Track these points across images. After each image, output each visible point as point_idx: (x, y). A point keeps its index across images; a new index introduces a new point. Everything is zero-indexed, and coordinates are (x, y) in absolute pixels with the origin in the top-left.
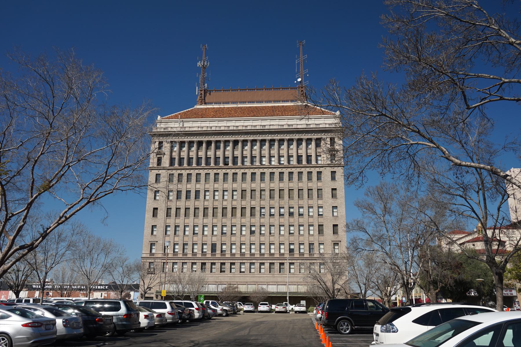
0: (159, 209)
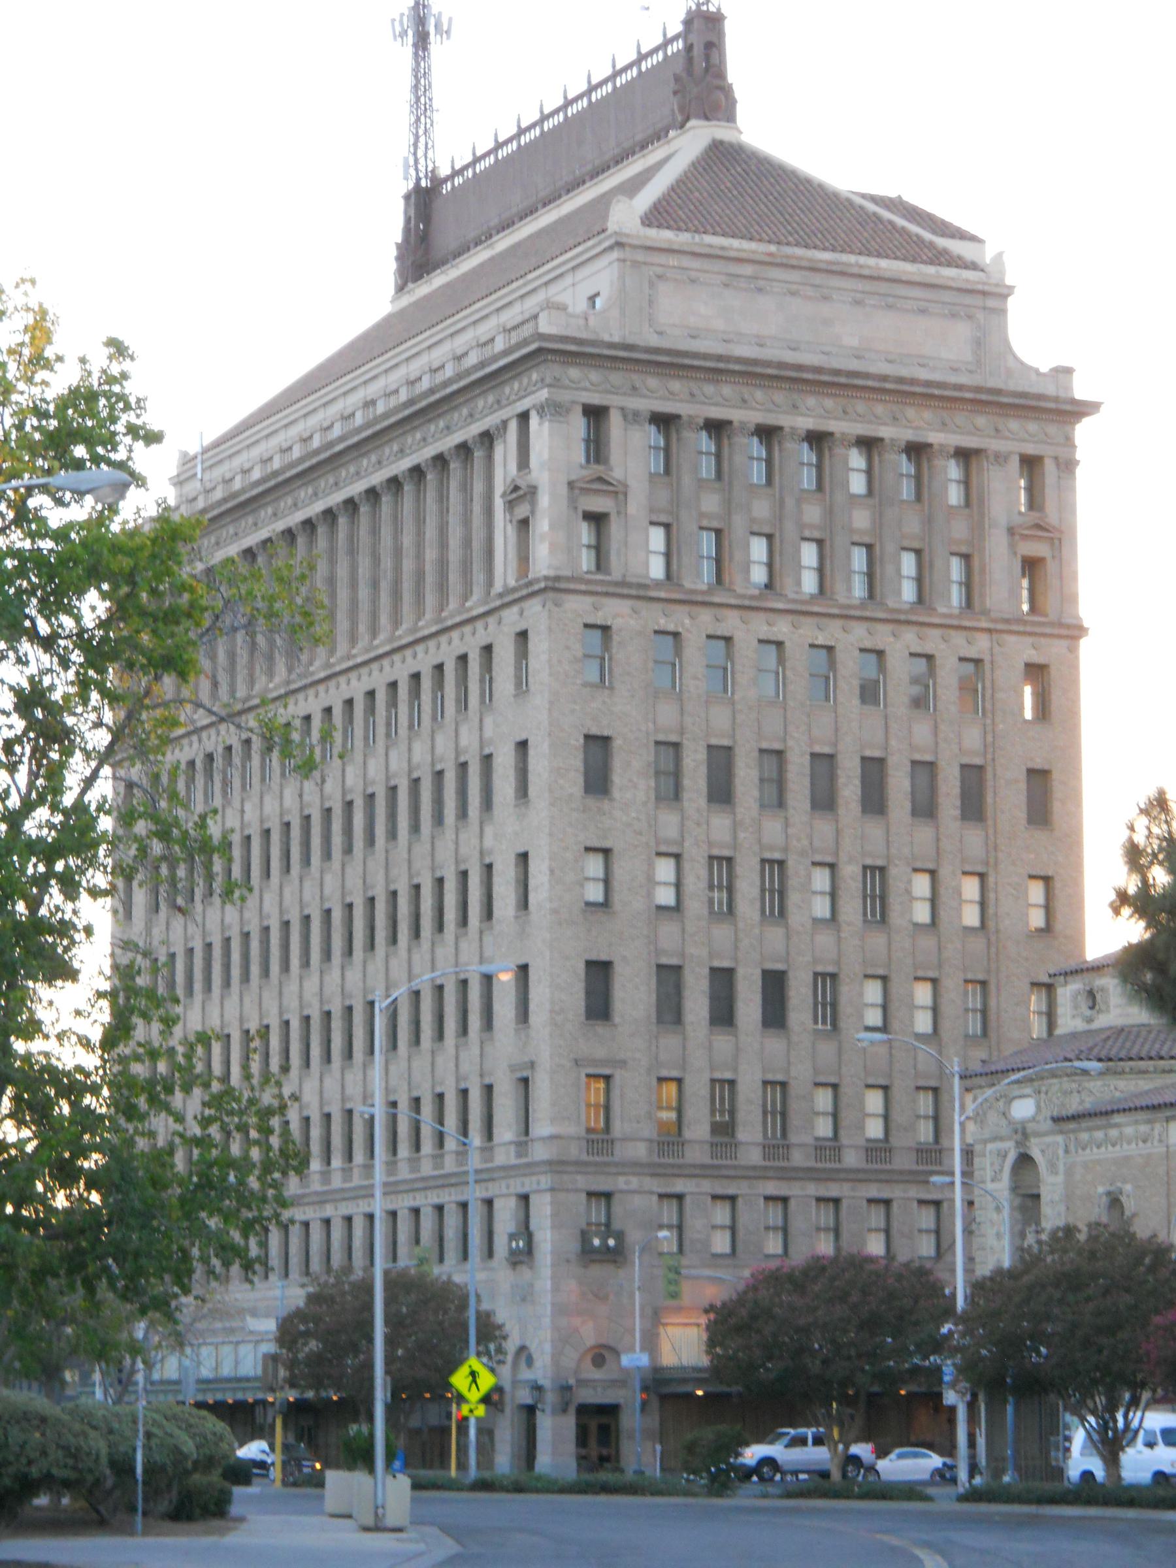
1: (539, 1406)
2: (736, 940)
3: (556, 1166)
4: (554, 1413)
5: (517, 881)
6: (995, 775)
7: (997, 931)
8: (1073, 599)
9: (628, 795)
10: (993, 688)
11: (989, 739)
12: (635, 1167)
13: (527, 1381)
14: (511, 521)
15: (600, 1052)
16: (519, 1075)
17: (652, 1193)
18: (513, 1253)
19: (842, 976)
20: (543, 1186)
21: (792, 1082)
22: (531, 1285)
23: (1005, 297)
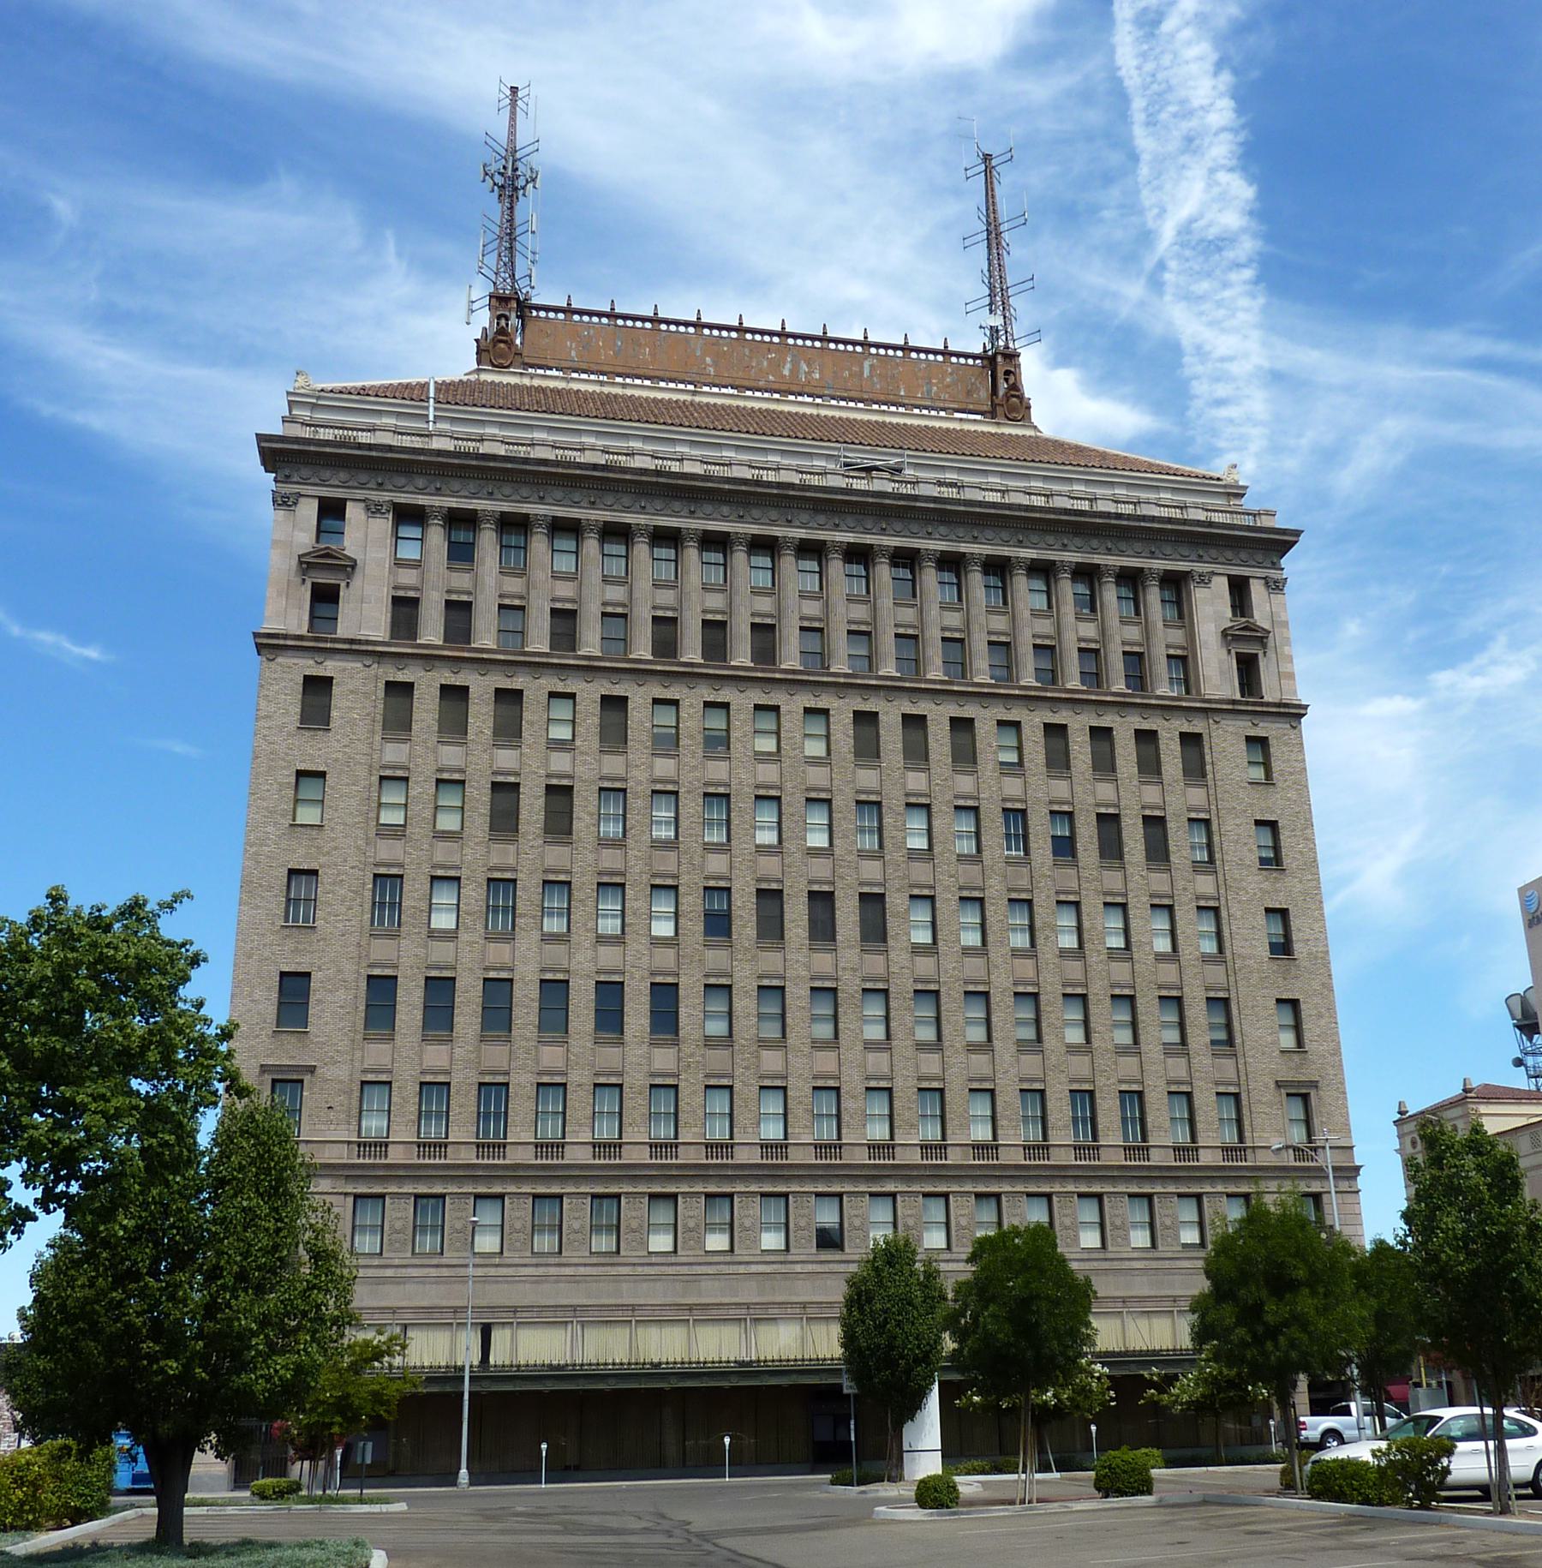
0: (325, 877)
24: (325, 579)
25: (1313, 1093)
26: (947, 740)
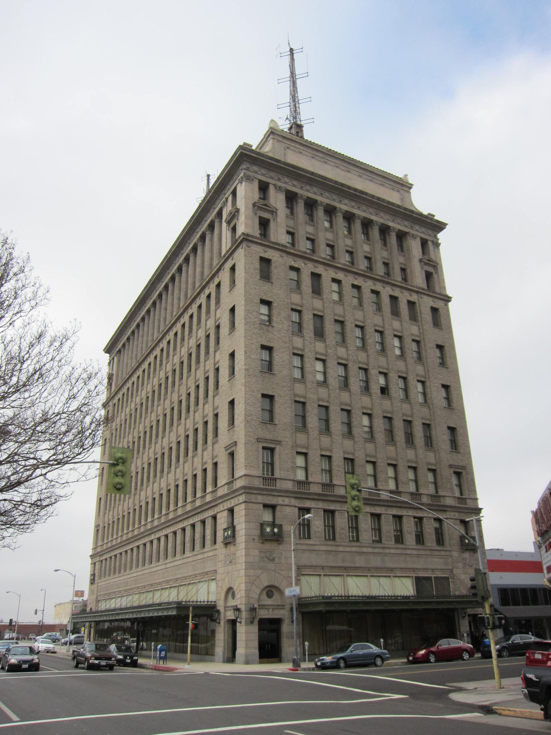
1: (238, 620)
2: (329, 394)
3: (247, 490)
4: (246, 624)
5: (230, 366)
6: (425, 344)
7: (432, 404)
8: (444, 288)
9: (280, 326)
10: (420, 313)
11: (421, 331)
12: (286, 493)
13: (232, 606)
14: (229, 230)
15: (269, 437)
16: (229, 451)
17: (295, 506)
18: (225, 538)
19: (374, 415)
20: (241, 501)
21: (356, 459)
22: (235, 554)
23: (411, 188)
24: (266, 215)
25: (464, 472)
26: (310, 281)
